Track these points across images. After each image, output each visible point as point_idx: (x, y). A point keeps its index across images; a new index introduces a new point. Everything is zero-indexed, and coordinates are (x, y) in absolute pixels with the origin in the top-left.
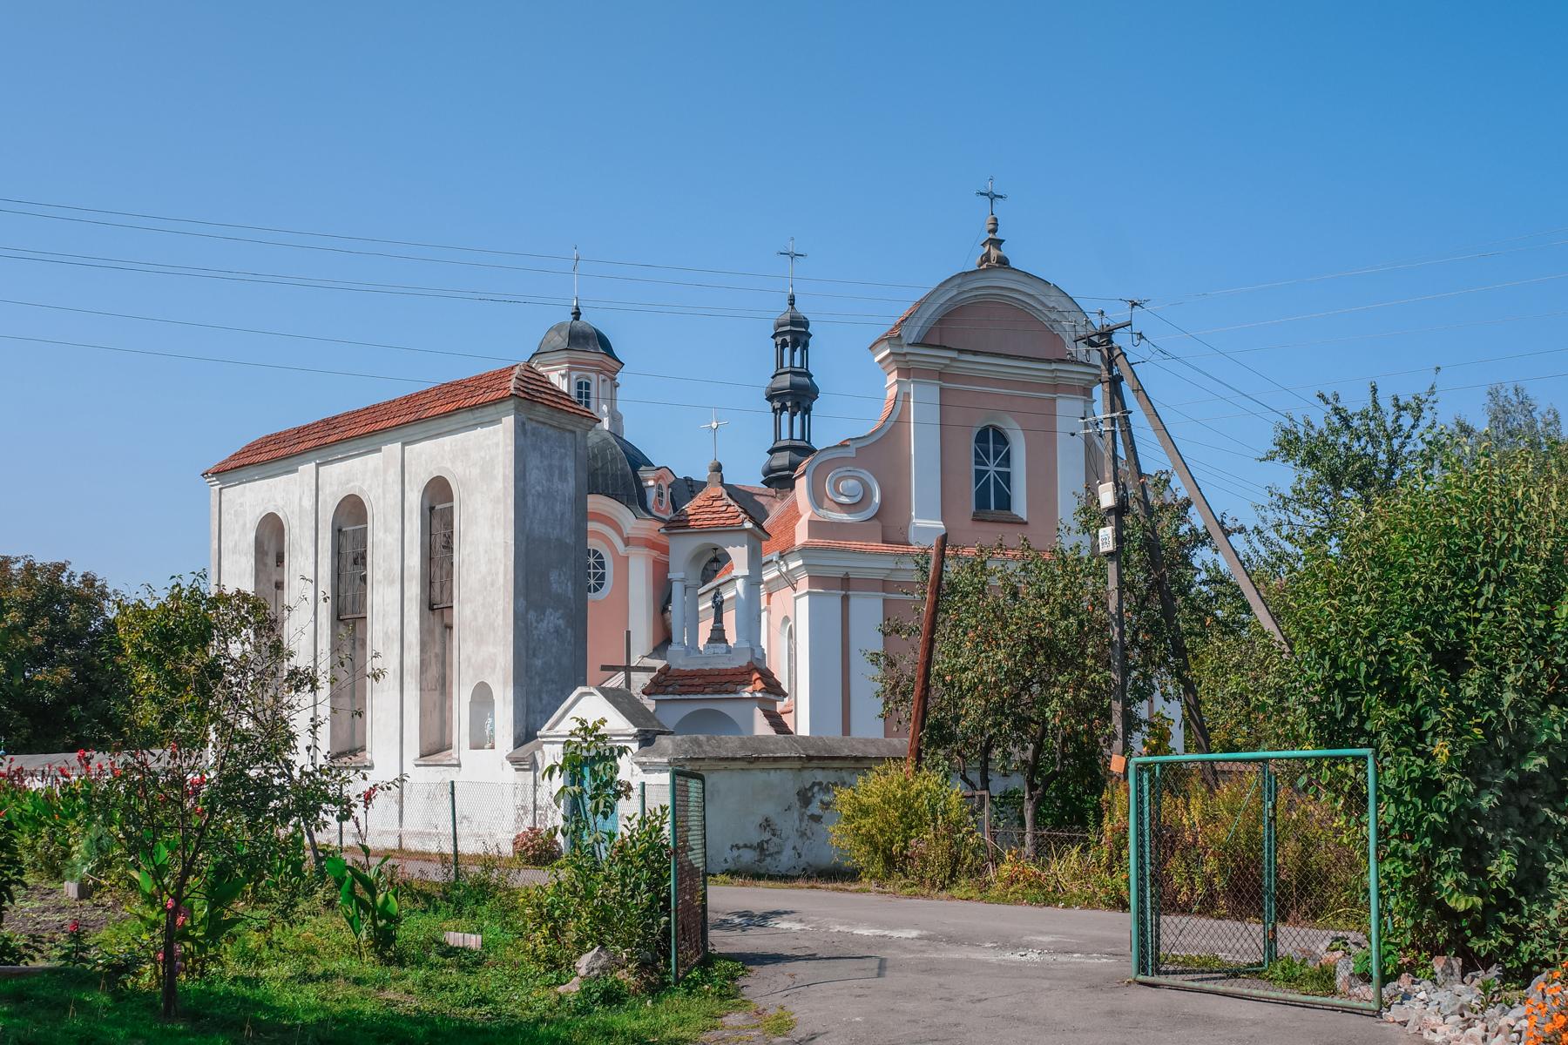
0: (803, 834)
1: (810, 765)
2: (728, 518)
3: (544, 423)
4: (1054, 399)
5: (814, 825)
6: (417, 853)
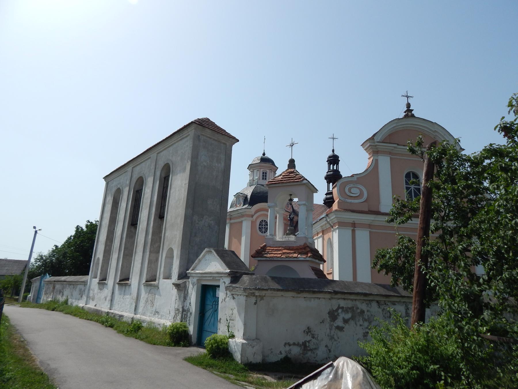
0: (332, 338)
1: (336, 296)
2: (296, 179)
3: (211, 138)
5: (340, 333)
6: (340, 292)
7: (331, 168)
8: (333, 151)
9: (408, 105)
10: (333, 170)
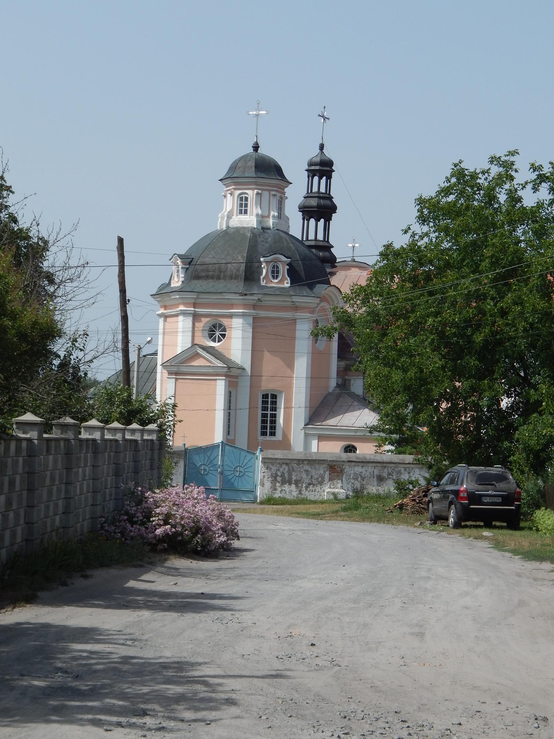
7: (315, 189)
8: (322, 147)
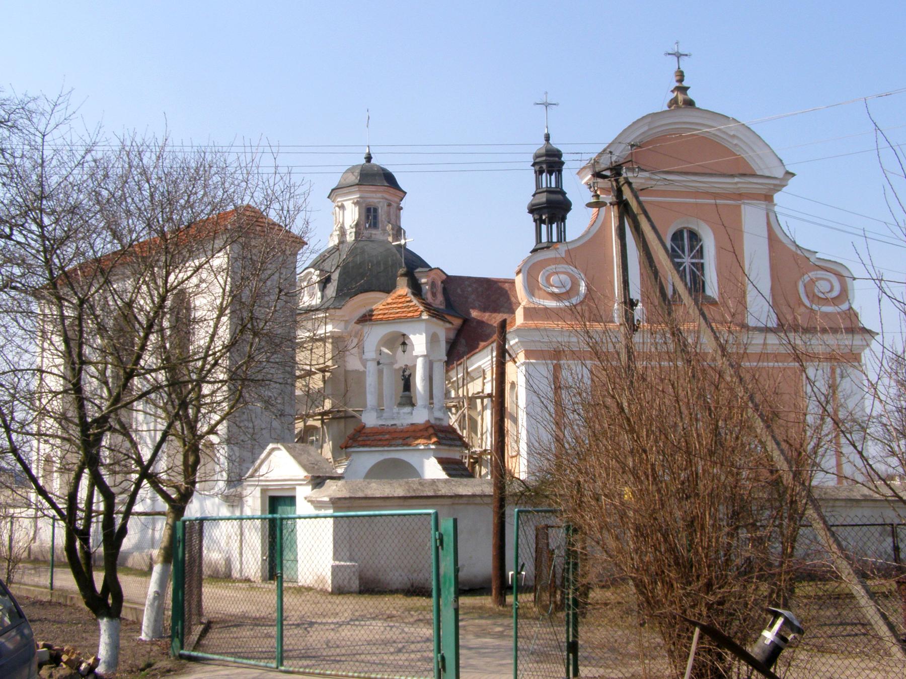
4: (739, 206)
8: (547, 138)
9: (681, 76)
10: (549, 191)
